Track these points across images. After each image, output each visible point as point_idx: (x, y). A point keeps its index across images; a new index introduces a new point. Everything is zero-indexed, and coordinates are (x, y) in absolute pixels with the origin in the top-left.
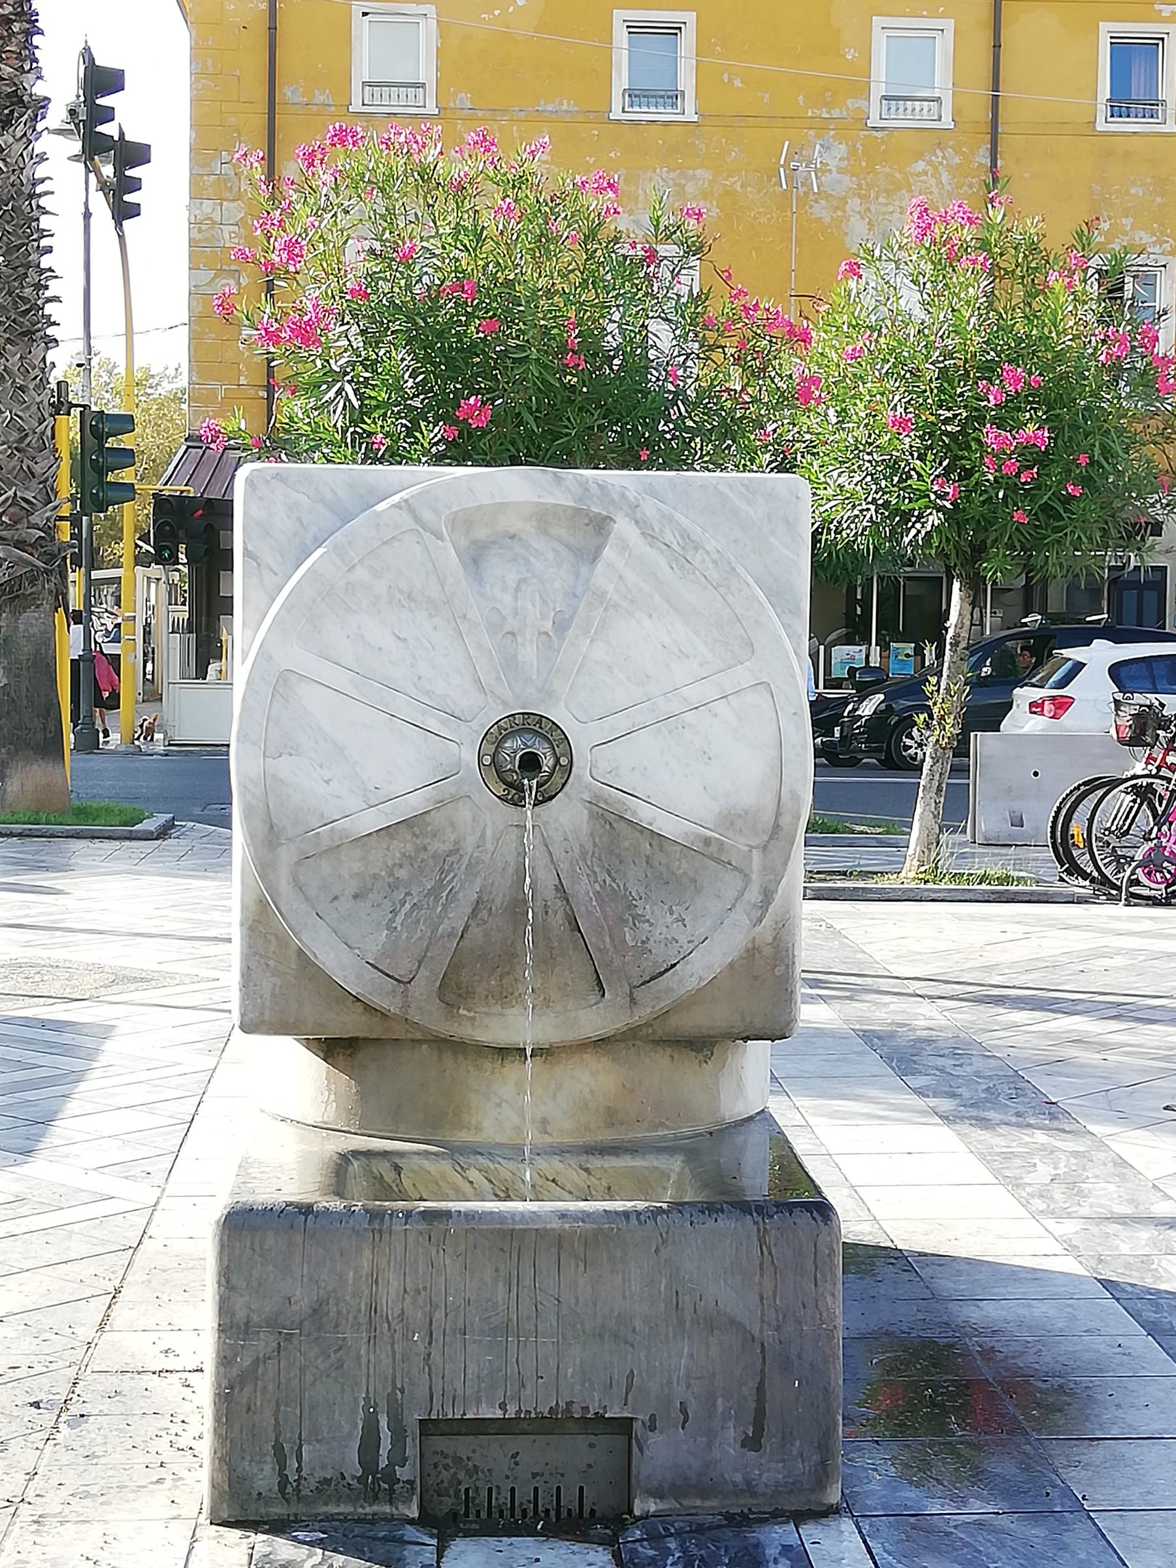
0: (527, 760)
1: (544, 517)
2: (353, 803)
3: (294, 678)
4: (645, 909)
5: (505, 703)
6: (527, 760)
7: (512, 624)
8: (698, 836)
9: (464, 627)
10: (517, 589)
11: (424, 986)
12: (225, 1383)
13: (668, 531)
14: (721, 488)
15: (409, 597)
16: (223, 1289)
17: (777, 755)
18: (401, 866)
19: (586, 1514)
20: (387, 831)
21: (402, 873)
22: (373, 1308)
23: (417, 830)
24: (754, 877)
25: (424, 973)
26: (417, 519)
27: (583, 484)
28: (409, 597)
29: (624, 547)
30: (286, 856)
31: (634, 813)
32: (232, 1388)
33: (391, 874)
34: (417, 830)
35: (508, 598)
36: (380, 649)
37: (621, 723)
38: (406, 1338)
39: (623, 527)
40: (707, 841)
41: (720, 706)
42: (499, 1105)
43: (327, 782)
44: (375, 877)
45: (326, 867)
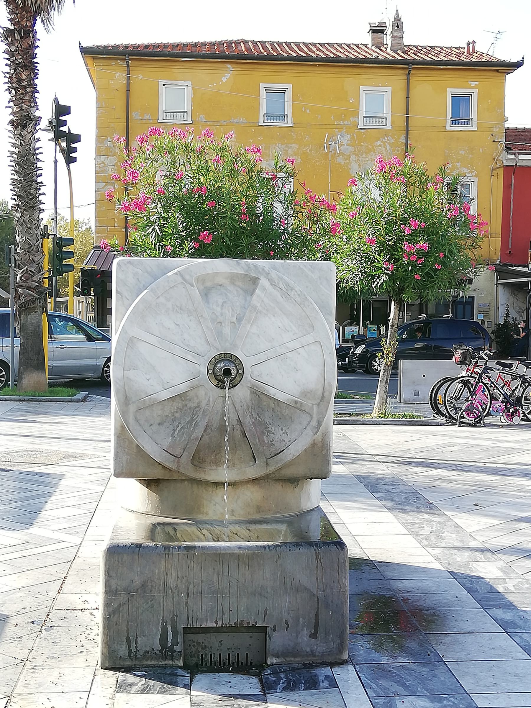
0: (226, 371)
1: (233, 278)
2: (159, 388)
3: (135, 340)
5: (218, 350)
6: (226, 371)
7: (220, 319)
10: (222, 305)
11: (185, 459)
14: (301, 266)
18: (177, 412)
21: (177, 415)
22: (165, 584)
24: (314, 416)
25: (186, 453)
27: (248, 265)
29: (264, 289)
30: (132, 408)
31: (268, 392)
32: (110, 615)
35: (219, 309)
37: (263, 357)
39: (264, 281)
40: (296, 402)
41: (301, 350)
44: (167, 416)
45: (147, 412)
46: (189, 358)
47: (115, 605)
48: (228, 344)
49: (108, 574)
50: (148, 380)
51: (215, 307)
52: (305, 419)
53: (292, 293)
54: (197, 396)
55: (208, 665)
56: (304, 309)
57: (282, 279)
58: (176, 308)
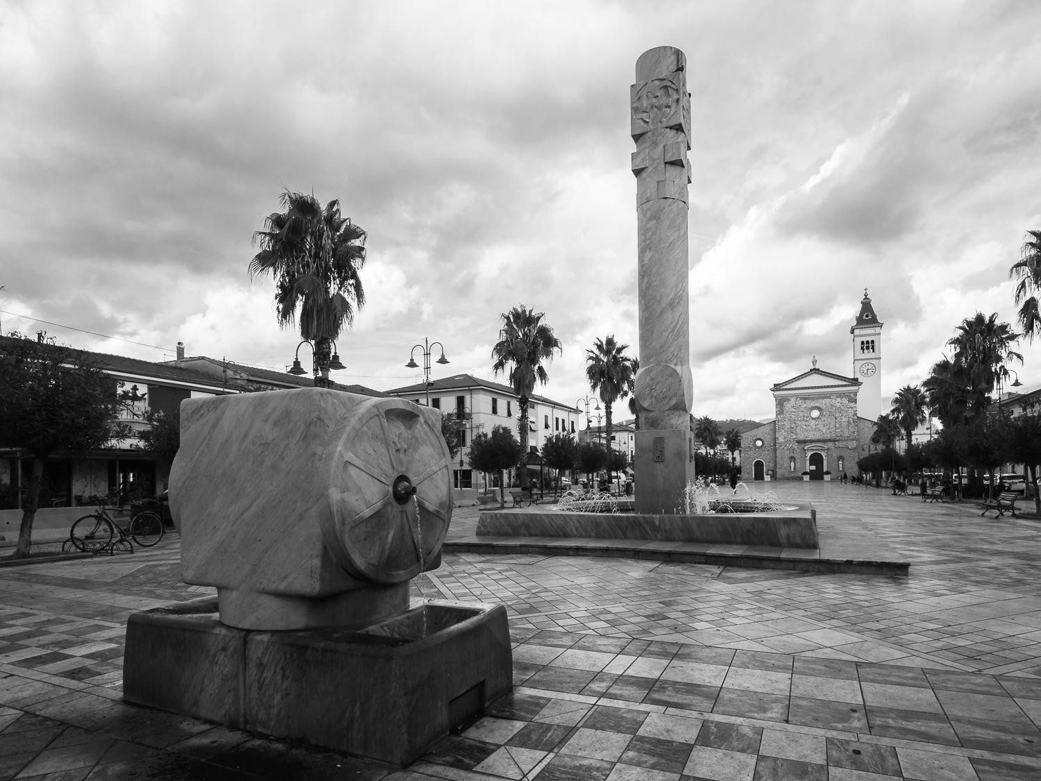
0: (402, 492)
3: (348, 464)
6: (402, 492)
9: (389, 448)
20: (372, 517)
35: (397, 439)
39: (421, 419)
40: (438, 511)
46: (383, 480)
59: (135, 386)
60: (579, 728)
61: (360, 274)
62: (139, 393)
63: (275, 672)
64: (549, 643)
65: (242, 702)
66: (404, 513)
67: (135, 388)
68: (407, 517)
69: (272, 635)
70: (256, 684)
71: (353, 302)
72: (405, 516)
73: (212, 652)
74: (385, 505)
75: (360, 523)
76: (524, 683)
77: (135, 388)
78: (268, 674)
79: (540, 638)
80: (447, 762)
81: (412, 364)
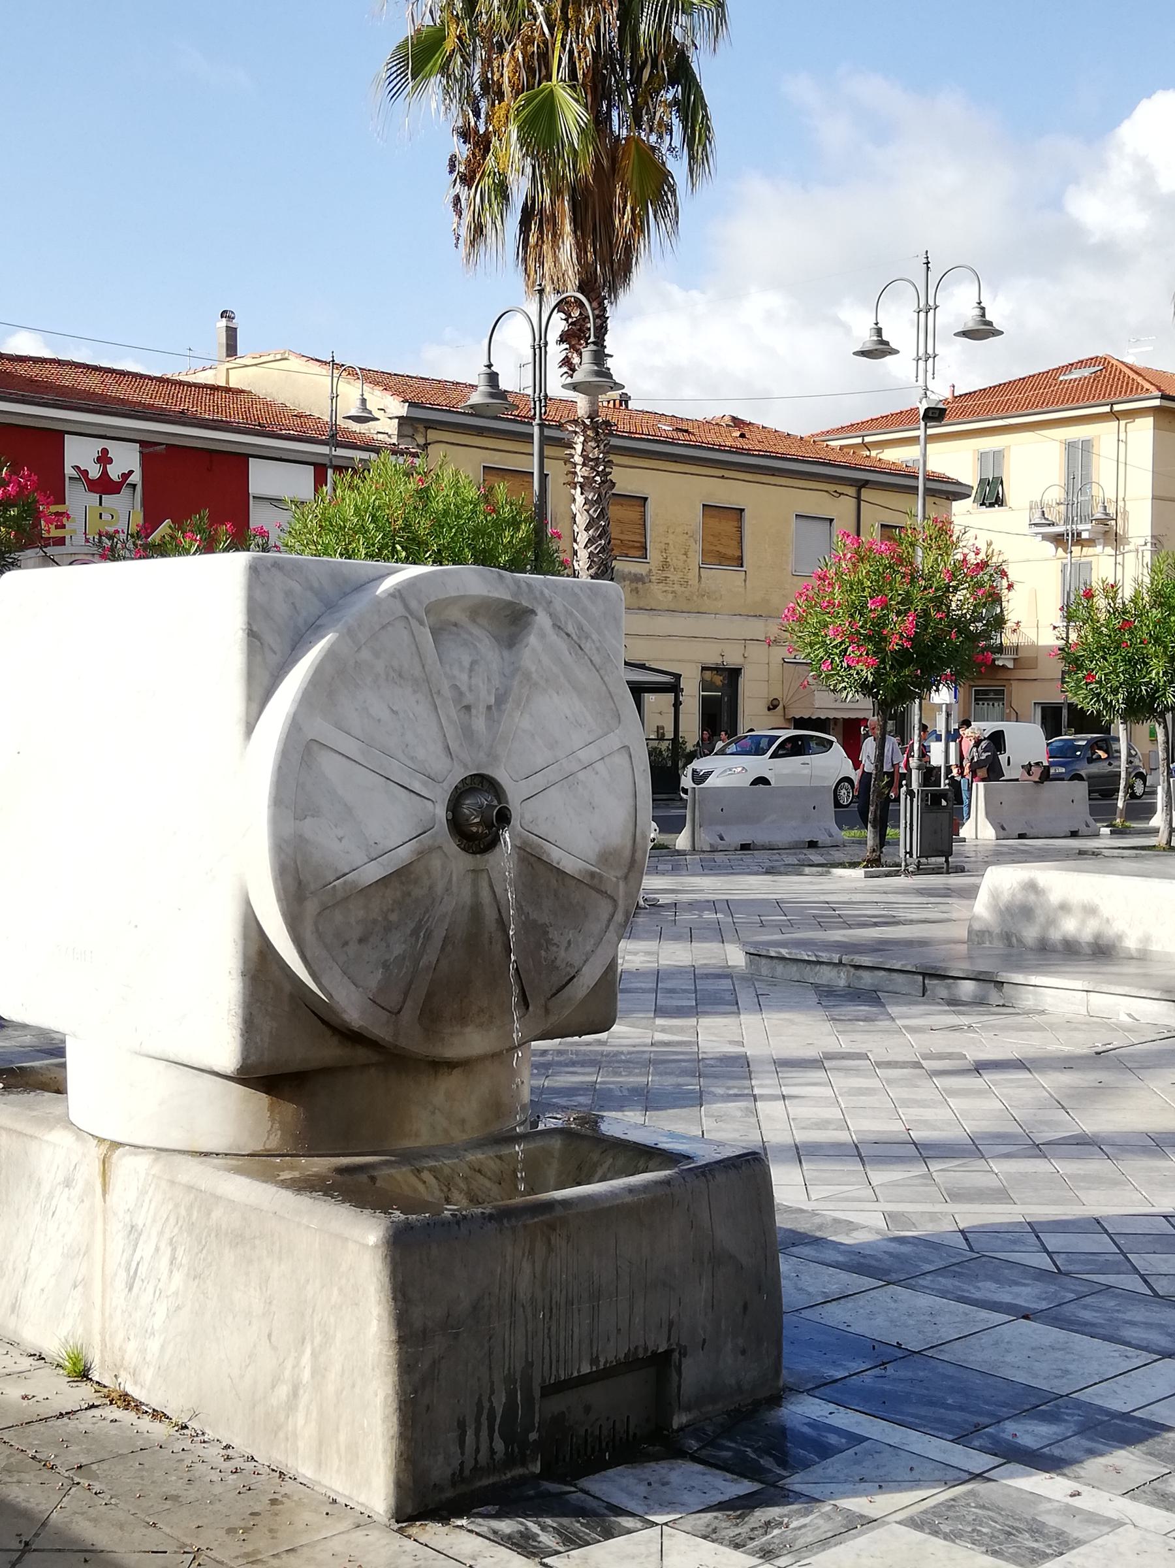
0: (477, 814)
1: (480, 609)
2: (359, 857)
3: (315, 747)
4: (554, 935)
5: (465, 766)
6: (477, 814)
7: (469, 698)
8: (587, 871)
9: (438, 702)
10: (471, 670)
11: (408, 1015)
12: (409, 1389)
13: (570, 623)
14: (577, 590)
15: (400, 676)
16: (399, 1303)
17: (633, 803)
18: (393, 911)
19: (631, 1438)
20: (384, 881)
21: (393, 917)
22: (514, 1296)
23: (403, 879)
24: (621, 902)
25: (409, 1003)
26: (406, 606)
27: (517, 582)
28: (400, 676)
29: (542, 635)
30: (311, 907)
31: (549, 855)
32: (416, 1392)
33: (386, 918)
34: (403, 879)
35: (465, 677)
36: (379, 720)
37: (539, 780)
38: (535, 1316)
39: (542, 619)
40: (592, 875)
41: (599, 766)
42: (433, 1113)
43: (340, 839)
44: (375, 921)
45: (338, 916)
46: (417, 787)
47: (423, 1365)
48: (482, 754)
49: (404, 1295)
50: (340, 839)
51: (456, 672)
52: (604, 908)
53: (587, 646)
54: (428, 872)
55: (567, 1459)
56: (606, 678)
57: (571, 614)
58: (392, 674)
59: (105, 451)
60: (888, 1523)
61: (703, 65)
62: (114, 472)
63: (157, 1249)
64: (977, 1295)
65: (97, 1314)
66: (485, 875)
67: (104, 459)
68: (491, 886)
69: (156, 1160)
70: (122, 1276)
71: (677, 167)
72: (484, 884)
73: (46, 1189)
74: (422, 854)
75: (346, 899)
76: (821, 1387)
77: (104, 459)
78: (145, 1250)
79: (955, 1275)
80: (495, 1532)
81: (880, 349)
